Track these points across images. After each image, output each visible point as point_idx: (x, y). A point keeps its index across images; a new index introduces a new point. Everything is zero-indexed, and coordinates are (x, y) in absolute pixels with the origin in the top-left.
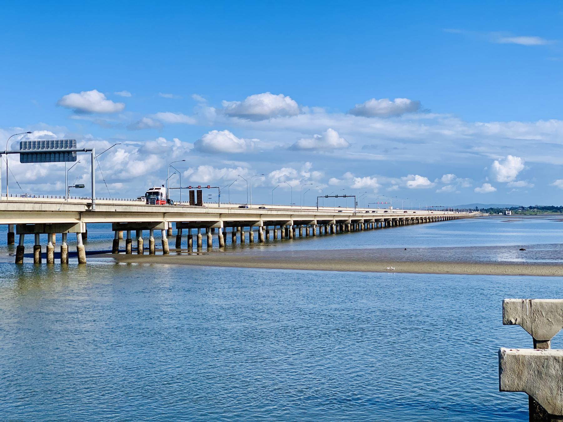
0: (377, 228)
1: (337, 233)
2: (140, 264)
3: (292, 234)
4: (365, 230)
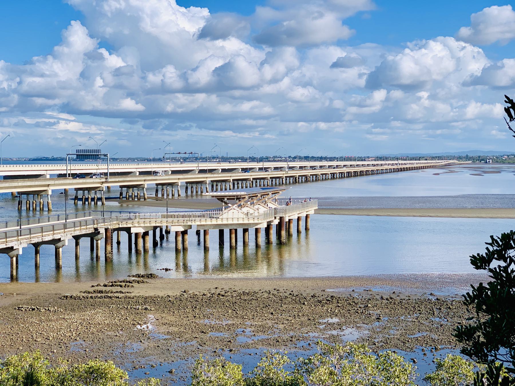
0: (382, 173)
1: (347, 177)
2: (127, 205)
4: (371, 174)
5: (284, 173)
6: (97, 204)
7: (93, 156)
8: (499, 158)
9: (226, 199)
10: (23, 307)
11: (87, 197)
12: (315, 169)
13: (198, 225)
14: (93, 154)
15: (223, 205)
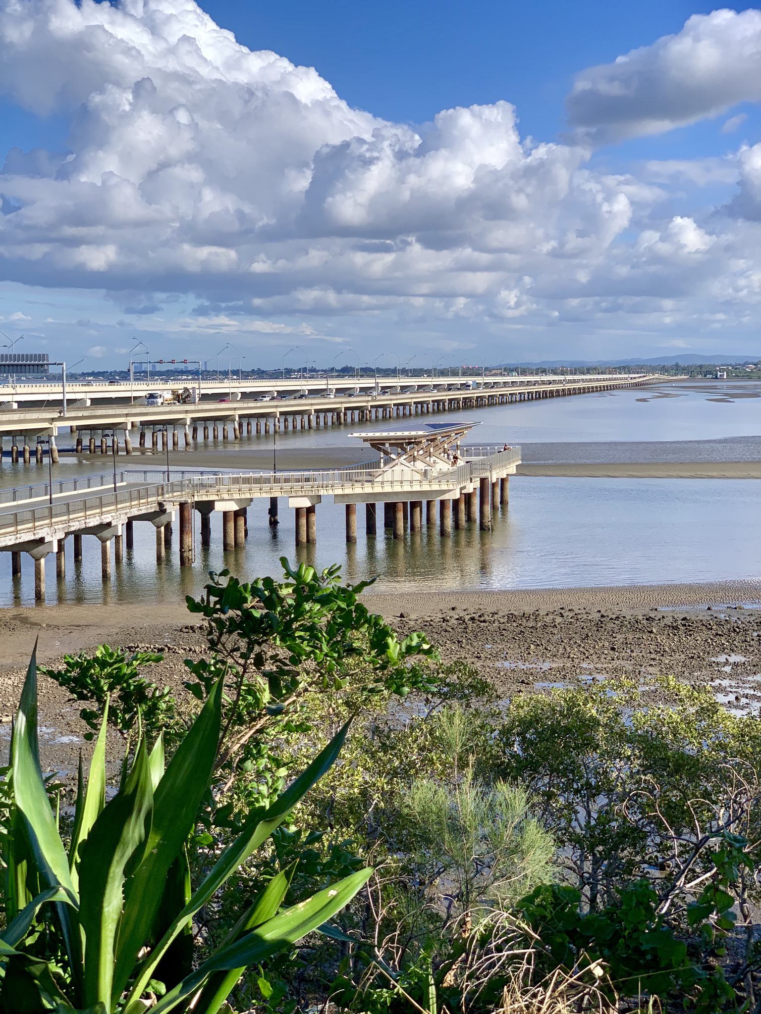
0: (511, 402)
3: (368, 417)
5: (370, 398)
6: (42, 461)
7: (27, 367)
8: (739, 368)
9: (387, 445)
10: (138, 647)
11: (21, 449)
12: (350, 395)
13: (336, 495)
14: (32, 362)
15: (382, 456)
